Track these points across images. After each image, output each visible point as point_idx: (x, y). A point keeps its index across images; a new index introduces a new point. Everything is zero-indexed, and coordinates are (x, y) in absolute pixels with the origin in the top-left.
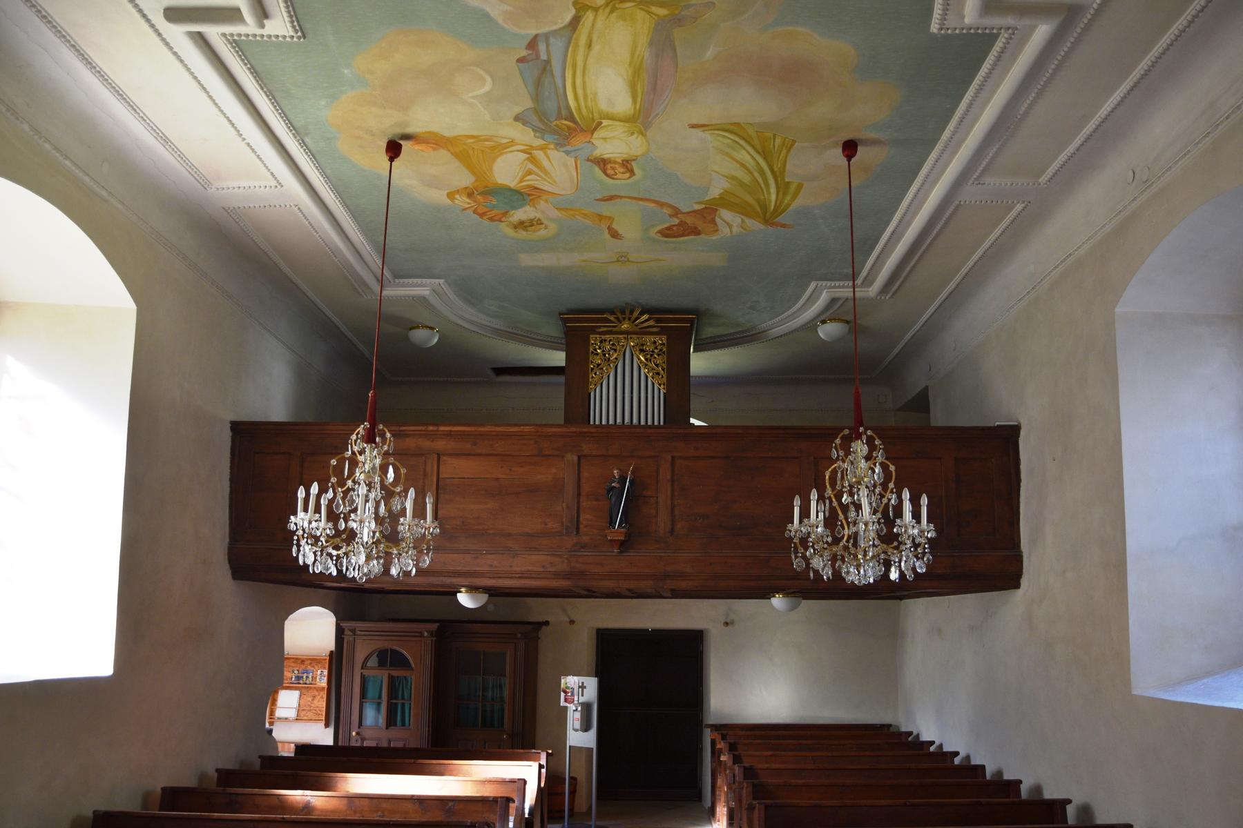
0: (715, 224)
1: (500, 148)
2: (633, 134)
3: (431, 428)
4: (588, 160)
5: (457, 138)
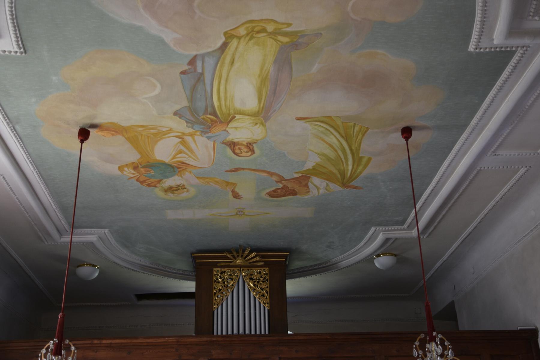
0: (308, 187)
1: (160, 134)
2: (256, 124)
3: (96, 341)
4: (223, 143)
5: (130, 128)
